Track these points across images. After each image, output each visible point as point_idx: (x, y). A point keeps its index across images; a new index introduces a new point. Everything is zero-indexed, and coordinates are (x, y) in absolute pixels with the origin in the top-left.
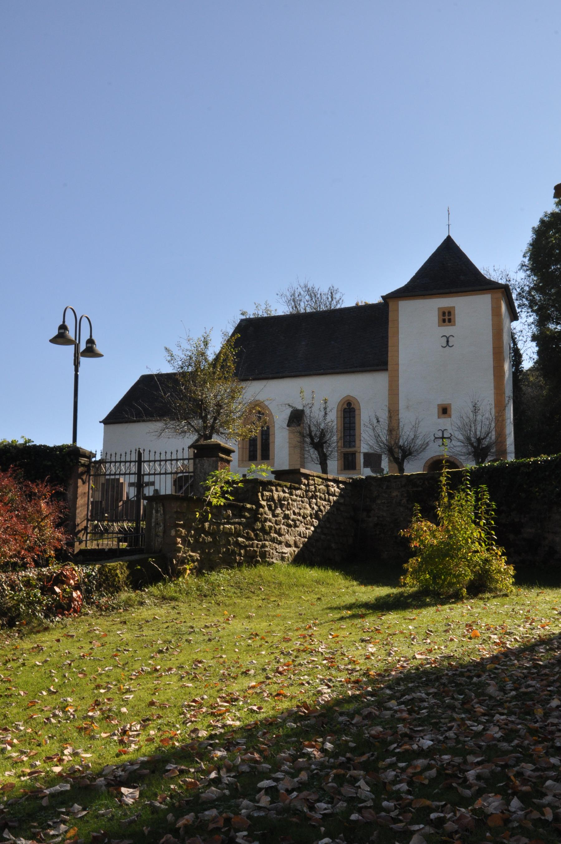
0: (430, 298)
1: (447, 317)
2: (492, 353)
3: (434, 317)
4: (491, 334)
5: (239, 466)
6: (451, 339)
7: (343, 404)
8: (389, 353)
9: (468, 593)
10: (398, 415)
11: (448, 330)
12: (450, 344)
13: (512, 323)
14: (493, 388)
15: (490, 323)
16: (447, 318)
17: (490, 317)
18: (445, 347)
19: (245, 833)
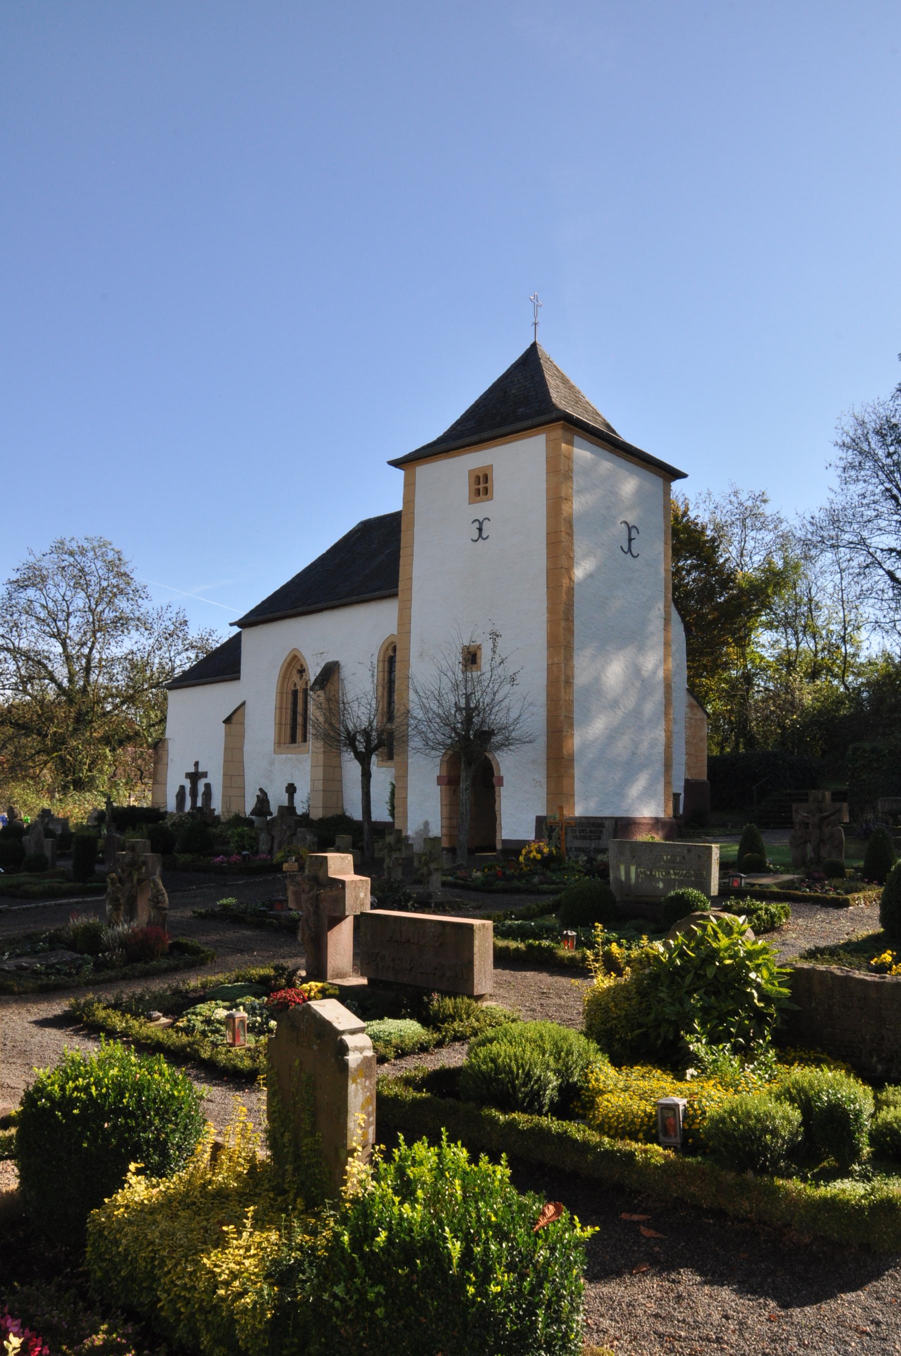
0: (458, 456)
1: (481, 486)
2: (544, 546)
3: (463, 487)
4: (545, 508)
5: (275, 752)
6: (486, 525)
7: (387, 649)
8: (401, 559)
9: (725, 883)
10: (408, 669)
11: (482, 509)
12: (484, 536)
13: (396, 506)
14: (545, 611)
15: (544, 486)
16: (481, 486)
17: (544, 477)
18: (476, 541)
19: (787, 1018)
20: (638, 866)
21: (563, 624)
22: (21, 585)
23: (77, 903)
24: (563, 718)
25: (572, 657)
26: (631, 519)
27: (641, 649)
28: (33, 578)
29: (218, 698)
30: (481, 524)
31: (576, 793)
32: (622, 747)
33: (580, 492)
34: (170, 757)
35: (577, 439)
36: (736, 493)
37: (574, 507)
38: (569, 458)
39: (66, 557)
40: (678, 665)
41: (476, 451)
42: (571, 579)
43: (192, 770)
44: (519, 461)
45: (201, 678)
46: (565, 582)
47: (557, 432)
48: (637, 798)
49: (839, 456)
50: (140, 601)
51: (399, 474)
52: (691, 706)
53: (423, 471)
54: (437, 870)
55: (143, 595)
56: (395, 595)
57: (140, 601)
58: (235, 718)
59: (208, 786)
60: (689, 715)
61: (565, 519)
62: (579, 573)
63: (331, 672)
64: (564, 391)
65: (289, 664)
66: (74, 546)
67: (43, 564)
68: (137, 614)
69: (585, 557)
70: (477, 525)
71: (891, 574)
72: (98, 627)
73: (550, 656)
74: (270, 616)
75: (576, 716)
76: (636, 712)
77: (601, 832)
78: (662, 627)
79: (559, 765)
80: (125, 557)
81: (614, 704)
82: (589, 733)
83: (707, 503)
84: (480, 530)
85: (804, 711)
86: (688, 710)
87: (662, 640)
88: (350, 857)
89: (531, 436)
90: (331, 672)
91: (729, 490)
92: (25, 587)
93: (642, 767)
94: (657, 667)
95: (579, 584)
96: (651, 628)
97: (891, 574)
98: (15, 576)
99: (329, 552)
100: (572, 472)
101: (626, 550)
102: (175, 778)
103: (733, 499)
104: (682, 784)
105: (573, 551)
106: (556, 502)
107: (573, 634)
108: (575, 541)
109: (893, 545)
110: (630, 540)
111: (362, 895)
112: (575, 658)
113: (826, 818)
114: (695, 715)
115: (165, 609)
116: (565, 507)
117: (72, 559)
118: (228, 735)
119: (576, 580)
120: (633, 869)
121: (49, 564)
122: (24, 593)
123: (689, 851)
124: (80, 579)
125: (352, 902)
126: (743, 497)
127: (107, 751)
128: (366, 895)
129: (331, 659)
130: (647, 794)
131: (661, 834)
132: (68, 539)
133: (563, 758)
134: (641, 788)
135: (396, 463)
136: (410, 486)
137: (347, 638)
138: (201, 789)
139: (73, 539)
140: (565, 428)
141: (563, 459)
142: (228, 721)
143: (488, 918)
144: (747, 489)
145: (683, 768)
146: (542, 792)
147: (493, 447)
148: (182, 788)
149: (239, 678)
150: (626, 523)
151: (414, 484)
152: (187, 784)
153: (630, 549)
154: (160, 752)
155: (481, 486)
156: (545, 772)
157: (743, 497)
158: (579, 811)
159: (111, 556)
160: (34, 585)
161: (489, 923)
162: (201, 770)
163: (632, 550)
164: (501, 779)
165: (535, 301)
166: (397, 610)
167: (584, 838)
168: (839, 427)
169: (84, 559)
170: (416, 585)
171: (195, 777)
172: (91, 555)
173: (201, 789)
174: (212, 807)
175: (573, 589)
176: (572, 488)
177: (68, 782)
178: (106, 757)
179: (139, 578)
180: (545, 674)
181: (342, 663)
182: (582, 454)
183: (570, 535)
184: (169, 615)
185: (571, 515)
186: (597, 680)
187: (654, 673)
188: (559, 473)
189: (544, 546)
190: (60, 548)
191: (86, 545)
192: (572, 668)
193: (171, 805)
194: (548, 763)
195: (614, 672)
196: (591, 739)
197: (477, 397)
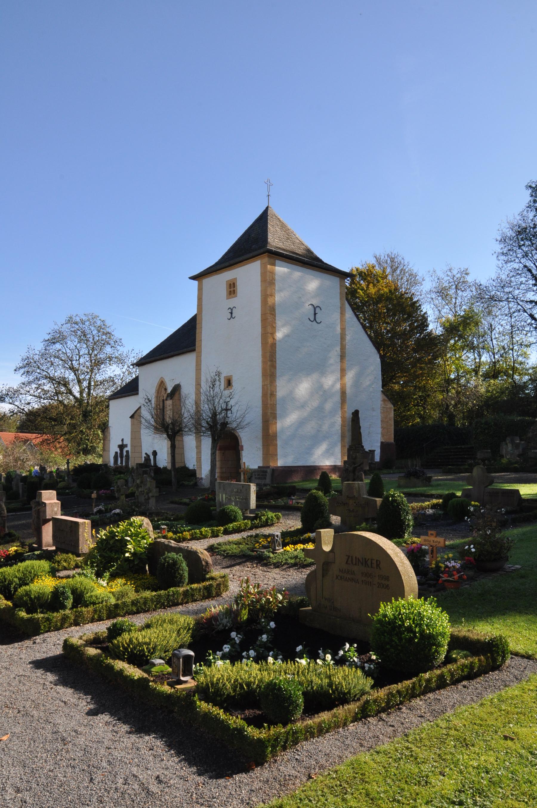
0: (222, 273)
1: (232, 289)
3: (223, 290)
12: (233, 317)
15: (260, 289)
16: (232, 289)
20: (226, 494)
21: (269, 363)
22: (53, 341)
23: (12, 515)
24: (269, 414)
25: (275, 381)
26: (315, 302)
27: (323, 373)
28: (57, 338)
29: (129, 404)
30: (232, 310)
31: (278, 453)
32: (310, 428)
33: (281, 290)
34: (111, 436)
35: (277, 261)
36: (450, 270)
37: (276, 299)
38: (273, 273)
39: (74, 325)
40: (375, 378)
41: (229, 270)
42: (274, 339)
43: (121, 443)
44: (249, 274)
45: (133, 391)
46: (270, 341)
47: (266, 259)
48: (322, 455)
49: (498, 247)
50: (118, 347)
51: (196, 283)
52: (384, 400)
53: (207, 281)
54: (153, 496)
55: (120, 344)
56: (194, 350)
57: (118, 347)
58: (136, 416)
59: (127, 452)
60: (383, 406)
61: (270, 306)
62: (279, 335)
63: (177, 388)
64: (280, 233)
65: (160, 386)
66: (78, 319)
67: (63, 330)
68: (117, 355)
69: (283, 326)
70: (230, 311)
71: (532, 316)
72: (97, 364)
73: (263, 381)
74: (153, 359)
75: (278, 412)
76: (320, 409)
77: (266, 475)
78: (339, 360)
79: (269, 439)
80: (108, 323)
81: (303, 406)
82: (286, 422)
83: (433, 277)
84: (231, 313)
85: (479, 397)
86: (382, 403)
87: (339, 368)
88: (54, 492)
89: (254, 262)
90: (177, 388)
91: (445, 269)
92: (54, 343)
93: (325, 438)
94: (335, 383)
95: (279, 341)
96: (332, 361)
97: (532, 316)
98: (47, 337)
99: (188, 322)
100: (275, 280)
101: (312, 319)
102: (114, 449)
103: (449, 273)
104: (379, 445)
105: (275, 323)
106: (266, 296)
107: (276, 368)
108: (277, 318)
109: (533, 298)
110: (315, 314)
111: (56, 509)
112: (277, 381)
113: (356, 467)
114: (386, 405)
115: (130, 351)
116: (270, 301)
117: (77, 327)
118: (133, 424)
119: (277, 339)
120: (224, 495)
121: (66, 329)
122: (54, 346)
123: (243, 487)
124: (83, 337)
125: (50, 513)
126: (455, 272)
127: (99, 432)
128: (58, 509)
129: (177, 383)
130: (328, 453)
131: (337, 474)
132: (75, 315)
133: (269, 435)
134: (324, 449)
135: (194, 278)
136: (200, 289)
137: (177, 371)
138: (125, 454)
139: (77, 315)
140: (269, 257)
141: (268, 273)
142: (132, 417)
143: (89, 519)
144: (457, 266)
145: (380, 436)
146: (260, 453)
147: (237, 268)
148: (116, 453)
149: (137, 394)
150: (312, 305)
151: (202, 289)
152: (118, 450)
153: (315, 319)
154: (106, 434)
155: (232, 289)
156: (261, 443)
157: (455, 272)
158: (280, 463)
159: (99, 323)
160: (58, 342)
161: (87, 521)
162: (125, 443)
163: (317, 320)
164: (242, 446)
165: (268, 183)
166: (195, 358)
167: (259, 478)
168: (500, 229)
169: (84, 326)
170: (204, 343)
171: (122, 447)
172: (87, 323)
173: (125, 454)
174: (367, 448)
175: (275, 344)
176: (275, 289)
177: (80, 450)
178: (99, 435)
179: (117, 335)
180: (261, 390)
181: (182, 384)
182: (281, 269)
183: (274, 315)
184: (133, 355)
185: (274, 304)
186: (291, 392)
187: (333, 386)
188: (268, 282)
189: (260, 321)
190: (70, 320)
191: (84, 318)
192: (276, 387)
193: (112, 463)
194: (263, 438)
195: (303, 388)
196: (289, 424)
197: (236, 239)
